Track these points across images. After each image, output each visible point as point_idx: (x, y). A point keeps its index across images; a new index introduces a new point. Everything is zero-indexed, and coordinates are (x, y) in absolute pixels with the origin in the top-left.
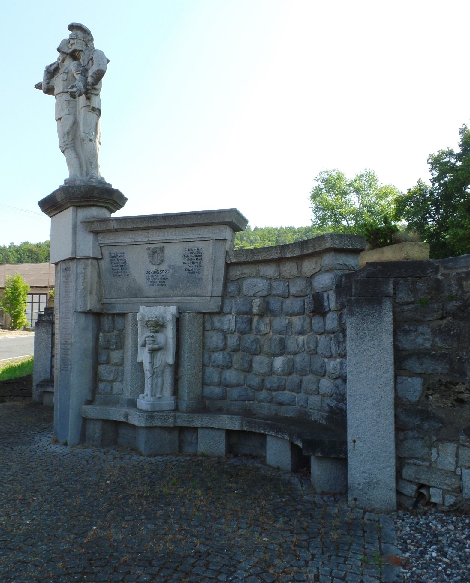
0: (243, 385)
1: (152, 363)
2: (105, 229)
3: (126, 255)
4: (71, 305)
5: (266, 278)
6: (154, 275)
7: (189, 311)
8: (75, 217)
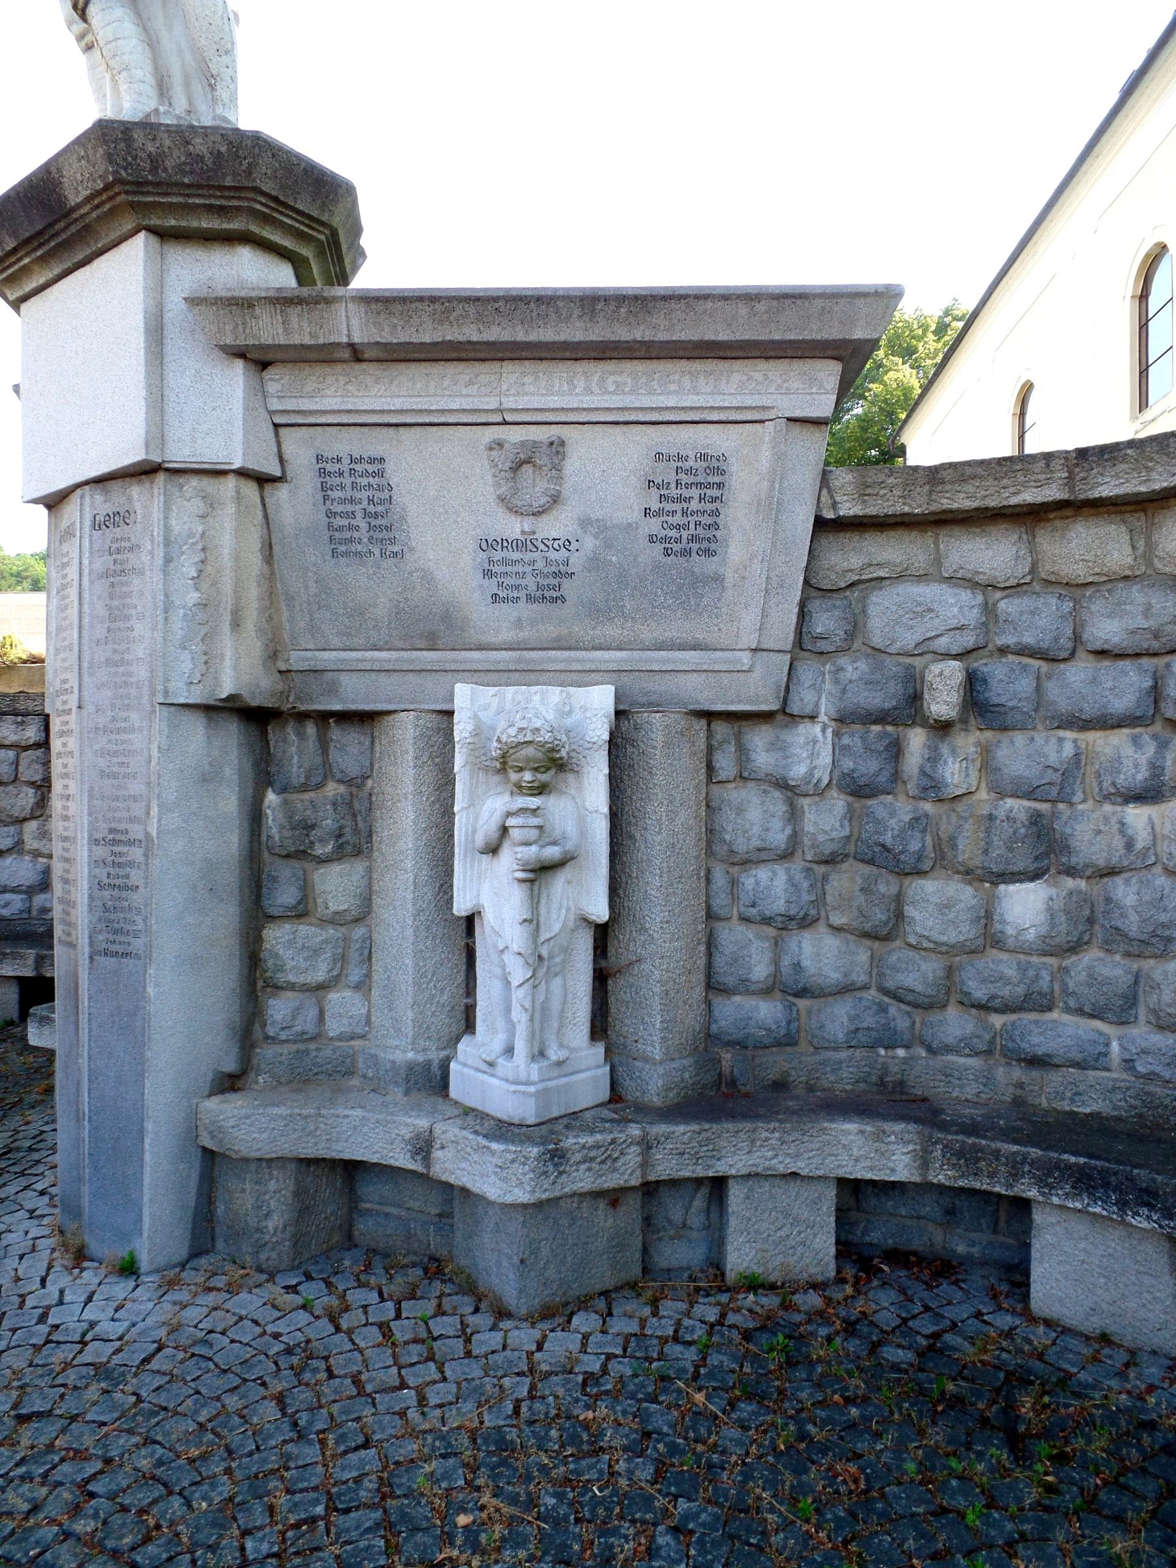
0: (865, 987)
1: (533, 922)
2: (307, 341)
3: (389, 467)
4: (141, 673)
5: (971, 583)
6: (515, 556)
7: (656, 706)
8: (157, 287)
